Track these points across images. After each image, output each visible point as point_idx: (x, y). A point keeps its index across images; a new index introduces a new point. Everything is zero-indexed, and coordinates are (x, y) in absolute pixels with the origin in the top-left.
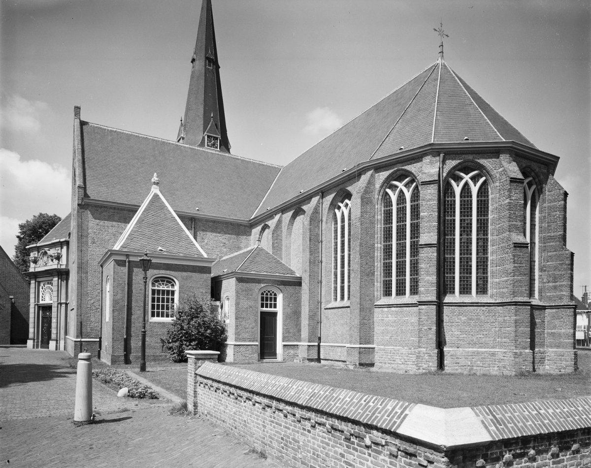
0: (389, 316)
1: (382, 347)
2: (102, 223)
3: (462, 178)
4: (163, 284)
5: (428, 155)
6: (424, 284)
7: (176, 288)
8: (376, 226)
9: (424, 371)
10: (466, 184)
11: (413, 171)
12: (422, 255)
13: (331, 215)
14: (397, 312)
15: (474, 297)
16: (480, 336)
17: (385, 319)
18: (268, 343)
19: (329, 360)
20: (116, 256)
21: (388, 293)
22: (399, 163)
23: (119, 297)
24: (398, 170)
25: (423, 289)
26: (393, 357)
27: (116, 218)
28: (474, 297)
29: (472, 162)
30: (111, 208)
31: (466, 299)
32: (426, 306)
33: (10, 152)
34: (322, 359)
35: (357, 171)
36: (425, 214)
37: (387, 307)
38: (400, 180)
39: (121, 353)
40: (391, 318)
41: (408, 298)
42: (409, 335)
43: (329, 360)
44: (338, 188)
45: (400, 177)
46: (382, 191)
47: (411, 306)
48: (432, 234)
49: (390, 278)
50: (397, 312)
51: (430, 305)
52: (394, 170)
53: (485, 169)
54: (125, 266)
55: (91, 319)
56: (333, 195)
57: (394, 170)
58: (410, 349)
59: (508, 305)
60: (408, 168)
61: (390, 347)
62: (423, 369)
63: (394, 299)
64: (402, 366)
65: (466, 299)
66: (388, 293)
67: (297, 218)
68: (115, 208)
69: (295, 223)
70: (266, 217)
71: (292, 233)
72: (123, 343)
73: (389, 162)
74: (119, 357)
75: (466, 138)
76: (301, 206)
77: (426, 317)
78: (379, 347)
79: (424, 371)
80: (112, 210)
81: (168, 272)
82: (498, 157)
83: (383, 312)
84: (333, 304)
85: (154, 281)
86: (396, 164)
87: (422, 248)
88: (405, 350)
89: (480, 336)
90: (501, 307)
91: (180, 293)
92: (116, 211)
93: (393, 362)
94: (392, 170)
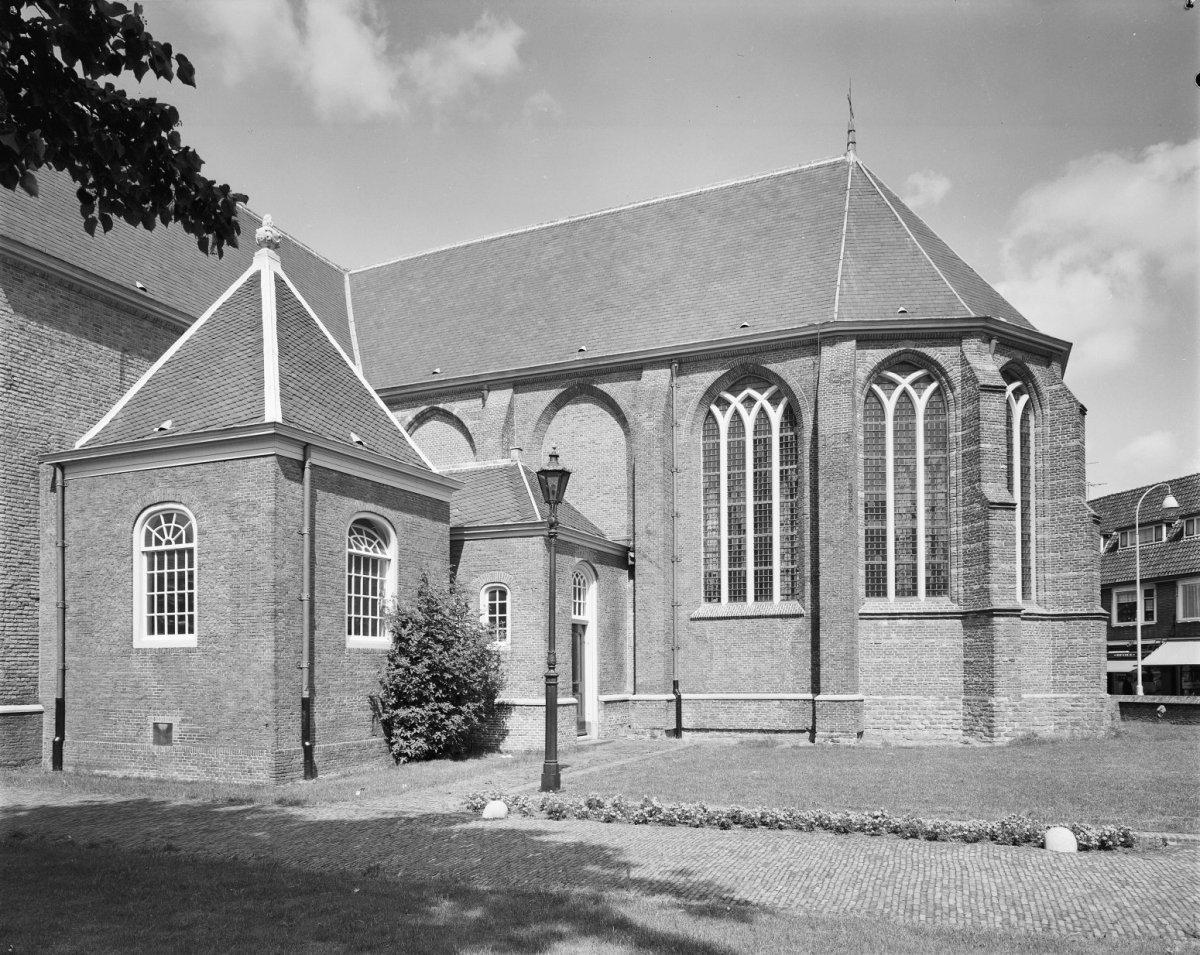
0: (893, 635)
1: (880, 697)
2: (33, 325)
3: (895, 384)
4: (370, 544)
5: (972, 337)
6: (997, 576)
7: (391, 552)
8: (1047, 465)
9: (1007, 739)
10: (905, 393)
11: (939, 360)
12: (994, 522)
13: (702, 417)
14: (910, 629)
15: (750, 606)
16: (1034, 672)
17: (884, 641)
18: (666, 692)
19: (712, 730)
20: (284, 446)
21: (712, 595)
22: (911, 339)
23: (285, 573)
24: (905, 352)
25: (996, 586)
26: (905, 715)
27: (74, 319)
28: (750, 606)
29: (1019, 365)
30: (61, 283)
31: (765, 608)
32: (1006, 619)
33: (1195, 141)
34: (688, 730)
35: (821, 334)
36: (988, 446)
37: (888, 619)
38: (904, 372)
39: (294, 744)
40: (896, 640)
41: (922, 602)
42: (936, 673)
43: (712, 730)
44: (736, 362)
45: (903, 365)
46: (867, 387)
47: (951, 618)
48: (999, 485)
49: (769, 567)
50: (910, 629)
51: (1012, 616)
52: (898, 349)
53: (1032, 382)
54: (301, 481)
55: (7, 640)
56: (718, 374)
57: (898, 349)
58: (943, 699)
59: (1080, 619)
60: (931, 352)
61: (897, 697)
62: (1006, 735)
63: (892, 602)
64: (926, 732)
65: (765, 608)
66: (876, 587)
67: (568, 407)
68: (70, 287)
69: (555, 421)
70: (450, 389)
71: (545, 441)
72: (298, 713)
73: (891, 332)
74: (290, 756)
75: (902, 309)
76: (593, 381)
77: (1006, 639)
78: (871, 697)
79: (1007, 739)
80: (63, 292)
81: (380, 509)
82: (1048, 366)
83: (877, 627)
84: (706, 609)
85: (355, 529)
86: (905, 339)
87: (994, 509)
88: (930, 702)
89: (1034, 672)
90: (1062, 623)
91: (400, 568)
92: (73, 296)
93: (905, 726)
94: (895, 350)
